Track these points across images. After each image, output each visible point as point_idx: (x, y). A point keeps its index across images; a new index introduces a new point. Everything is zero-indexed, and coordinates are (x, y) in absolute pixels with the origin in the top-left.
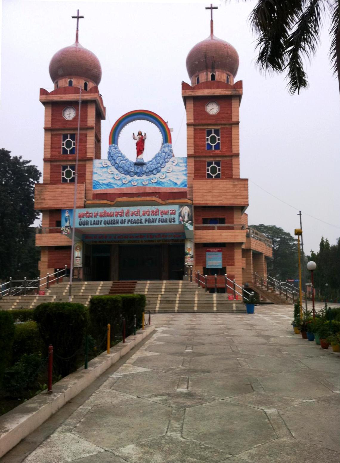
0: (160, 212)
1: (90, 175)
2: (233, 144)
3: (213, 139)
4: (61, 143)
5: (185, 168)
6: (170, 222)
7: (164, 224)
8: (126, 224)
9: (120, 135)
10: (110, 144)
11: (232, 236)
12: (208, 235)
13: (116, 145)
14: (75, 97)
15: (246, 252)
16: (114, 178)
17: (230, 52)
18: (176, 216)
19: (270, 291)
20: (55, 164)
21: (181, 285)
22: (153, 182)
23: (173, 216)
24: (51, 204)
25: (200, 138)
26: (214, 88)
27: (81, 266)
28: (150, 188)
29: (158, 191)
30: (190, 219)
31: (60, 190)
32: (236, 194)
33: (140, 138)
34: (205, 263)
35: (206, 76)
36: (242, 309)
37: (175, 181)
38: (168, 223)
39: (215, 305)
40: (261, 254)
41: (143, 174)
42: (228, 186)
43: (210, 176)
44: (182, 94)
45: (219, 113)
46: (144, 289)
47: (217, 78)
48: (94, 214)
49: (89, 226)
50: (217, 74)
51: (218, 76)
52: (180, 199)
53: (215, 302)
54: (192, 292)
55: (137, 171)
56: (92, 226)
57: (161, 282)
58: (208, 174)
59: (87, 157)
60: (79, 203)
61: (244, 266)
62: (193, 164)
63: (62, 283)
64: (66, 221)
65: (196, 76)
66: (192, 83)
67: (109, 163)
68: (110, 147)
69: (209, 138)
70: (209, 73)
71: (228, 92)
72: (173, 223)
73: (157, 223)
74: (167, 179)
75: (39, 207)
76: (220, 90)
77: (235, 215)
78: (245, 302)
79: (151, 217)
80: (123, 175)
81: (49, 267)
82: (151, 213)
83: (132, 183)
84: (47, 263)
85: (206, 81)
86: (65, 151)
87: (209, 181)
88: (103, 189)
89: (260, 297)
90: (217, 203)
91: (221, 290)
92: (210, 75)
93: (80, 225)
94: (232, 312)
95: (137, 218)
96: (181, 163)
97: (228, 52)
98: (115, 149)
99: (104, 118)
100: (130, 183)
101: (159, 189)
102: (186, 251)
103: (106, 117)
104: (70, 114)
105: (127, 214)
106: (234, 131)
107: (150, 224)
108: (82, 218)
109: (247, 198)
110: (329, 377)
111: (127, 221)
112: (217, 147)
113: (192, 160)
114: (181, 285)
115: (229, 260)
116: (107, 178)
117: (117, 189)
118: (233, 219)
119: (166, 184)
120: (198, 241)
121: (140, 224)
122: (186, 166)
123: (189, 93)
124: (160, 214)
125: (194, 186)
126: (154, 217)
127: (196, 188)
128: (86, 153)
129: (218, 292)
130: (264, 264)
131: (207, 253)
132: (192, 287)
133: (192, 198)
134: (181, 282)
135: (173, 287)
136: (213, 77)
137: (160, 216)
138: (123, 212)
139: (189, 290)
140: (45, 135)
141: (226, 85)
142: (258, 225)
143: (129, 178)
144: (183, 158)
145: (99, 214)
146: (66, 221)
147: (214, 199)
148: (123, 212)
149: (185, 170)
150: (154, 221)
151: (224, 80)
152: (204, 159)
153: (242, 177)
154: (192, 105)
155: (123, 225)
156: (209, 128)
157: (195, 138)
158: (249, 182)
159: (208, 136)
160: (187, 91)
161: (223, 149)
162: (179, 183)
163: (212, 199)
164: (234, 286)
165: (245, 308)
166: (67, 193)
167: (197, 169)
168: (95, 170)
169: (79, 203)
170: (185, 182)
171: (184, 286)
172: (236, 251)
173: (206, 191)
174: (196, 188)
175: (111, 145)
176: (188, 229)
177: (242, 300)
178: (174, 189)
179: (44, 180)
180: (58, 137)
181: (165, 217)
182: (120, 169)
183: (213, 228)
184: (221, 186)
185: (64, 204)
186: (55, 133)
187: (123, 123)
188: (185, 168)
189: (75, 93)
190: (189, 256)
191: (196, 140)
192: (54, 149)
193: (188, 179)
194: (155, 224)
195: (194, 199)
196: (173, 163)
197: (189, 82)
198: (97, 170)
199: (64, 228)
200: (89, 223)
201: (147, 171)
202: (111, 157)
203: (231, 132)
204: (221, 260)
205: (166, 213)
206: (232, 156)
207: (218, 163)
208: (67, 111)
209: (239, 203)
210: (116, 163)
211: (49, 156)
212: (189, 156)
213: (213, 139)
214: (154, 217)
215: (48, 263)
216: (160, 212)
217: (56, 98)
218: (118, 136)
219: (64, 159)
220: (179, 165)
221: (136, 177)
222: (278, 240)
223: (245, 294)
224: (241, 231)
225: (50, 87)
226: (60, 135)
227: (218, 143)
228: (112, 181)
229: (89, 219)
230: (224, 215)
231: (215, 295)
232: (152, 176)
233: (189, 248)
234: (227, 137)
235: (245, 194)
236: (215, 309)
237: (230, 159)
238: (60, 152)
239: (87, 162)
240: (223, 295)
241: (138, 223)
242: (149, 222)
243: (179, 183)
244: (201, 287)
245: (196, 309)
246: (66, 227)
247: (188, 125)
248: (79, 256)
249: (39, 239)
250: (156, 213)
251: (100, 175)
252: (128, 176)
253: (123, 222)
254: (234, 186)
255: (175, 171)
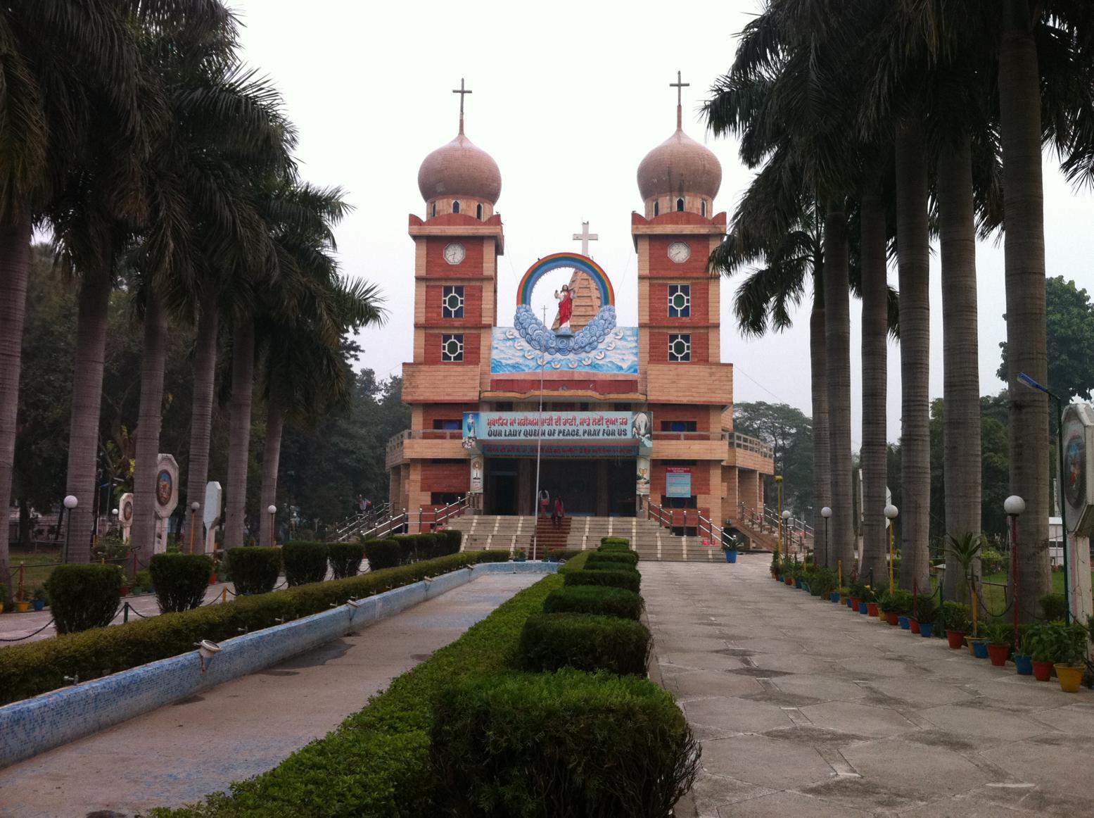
0: (604, 421)
1: (487, 352)
2: (710, 309)
3: (679, 300)
4: (441, 300)
5: (634, 344)
6: (620, 435)
7: (610, 437)
8: (556, 437)
9: (534, 290)
10: (518, 304)
11: (707, 449)
12: (670, 447)
13: (528, 306)
14: (465, 231)
15: (728, 470)
16: (524, 356)
17: (707, 166)
18: (628, 427)
19: (766, 532)
20: (431, 331)
21: (634, 523)
22: (586, 364)
23: (623, 427)
24: (428, 394)
25: (659, 299)
26: (682, 224)
27: (481, 491)
28: (580, 373)
29: (592, 379)
30: (648, 431)
31: (442, 374)
32: (713, 387)
33: (565, 296)
34: (664, 488)
35: (669, 202)
36: (720, 557)
37: (619, 364)
38: (617, 437)
39: (685, 552)
40: (754, 471)
41: (570, 351)
42: (702, 374)
43: (673, 357)
44: (632, 231)
45: (689, 261)
46: (584, 528)
47: (686, 206)
48: (509, 422)
49: (503, 438)
50: (687, 200)
51: (689, 203)
52: (628, 393)
53: (684, 548)
54: (651, 533)
55: (561, 346)
56: (506, 438)
57: (606, 519)
58: (671, 354)
59: (483, 322)
60: (472, 394)
61: (725, 495)
62: (648, 338)
63: (465, 517)
64: (470, 430)
65: (654, 201)
66: (647, 213)
67: (516, 334)
68: (518, 309)
69: (673, 298)
70: (674, 198)
71: (703, 230)
72: (623, 437)
73: (601, 437)
74: (608, 360)
75: (409, 398)
76: (692, 226)
77: (711, 417)
78: (724, 548)
79: (592, 428)
80: (538, 352)
81: (423, 489)
82: (591, 421)
83: (553, 364)
84: (419, 484)
85: (669, 211)
86: (447, 313)
87: (673, 367)
88: (507, 372)
89: (751, 543)
90: (685, 400)
91: (692, 532)
92: (676, 200)
93: (490, 435)
94: (708, 561)
95: (571, 428)
96: (629, 336)
97: (704, 166)
98: (527, 311)
99: (502, 254)
100: (548, 365)
101: (594, 375)
102: (639, 473)
103: (505, 251)
104: (455, 255)
105: (558, 420)
106: (712, 288)
107: (590, 437)
108: (492, 427)
109: (731, 393)
110: (1003, 798)
111: (557, 432)
112: (685, 312)
113: (646, 332)
114: (634, 523)
115: (701, 485)
116: (513, 355)
117: (529, 374)
118: (708, 423)
119: (605, 368)
120: (655, 456)
121: (575, 437)
122: (636, 341)
123: (644, 230)
124: (604, 423)
125: (649, 372)
126: (597, 427)
127: (652, 377)
128: (481, 316)
129: (689, 535)
130: (758, 487)
131: (668, 474)
132: (650, 527)
133: (646, 391)
134: (634, 519)
135: (624, 527)
136: (680, 204)
137: (605, 427)
138: (551, 419)
139: (646, 531)
140: (416, 287)
141: (701, 219)
142: (753, 402)
143: (548, 357)
144: (632, 328)
145: (517, 422)
146: (470, 430)
147: (680, 394)
148: (551, 419)
149: (636, 347)
150: (596, 433)
151: (698, 209)
152: (665, 331)
153: (724, 359)
154: (648, 247)
155: (552, 437)
156: (673, 283)
157: (650, 299)
158: (734, 369)
159: (671, 295)
160: (640, 226)
161: (695, 317)
162: (625, 366)
163: (676, 394)
164: (710, 528)
165: (725, 557)
166: (453, 378)
167: (653, 347)
168: (495, 344)
169: (472, 394)
170: (635, 365)
171: (639, 525)
172: (712, 472)
173: (666, 381)
174: (652, 377)
175: (520, 306)
176: (645, 446)
177: (721, 546)
178: (618, 375)
179: (414, 357)
180: (438, 290)
181: (612, 427)
182: (533, 342)
183: (678, 438)
184: (691, 373)
185: (448, 395)
186: (432, 283)
187: (538, 272)
188: (634, 344)
189: (464, 224)
190: (642, 480)
191: (653, 300)
192: (430, 310)
193: (640, 361)
194: (597, 437)
195: (649, 393)
196: (617, 335)
197: (642, 211)
198: (497, 344)
199: (467, 440)
200: (503, 434)
201: (576, 347)
202: (519, 323)
203: (708, 289)
204: (689, 485)
205: (613, 422)
206: (708, 327)
207: (686, 338)
208: (450, 249)
209: (718, 400)
210: (528, 334)
211: (422, 320)
212: (642, 326)
213: (679, 300)
214: (597, 427)
215: (422, 483)
216: (604, 421)
217: (436, 230)
218: (531, 291)
219: (447, 325)
220: (626, 340)
221: (558, 356)
222: (793, 431)
223: (724, 538)
224: (720, 442)
225: (422, 210)
226: (440, 287)
227: (687, 307)
228: (521, 361)
229: (503, 428)
230: (695, 418)
231: (684, 538)
232: (583, 355)
233: (643, 469)
234: (699, 298)
235: (727, 387)
236: (685, 556)
237: (706, 331)
238: (439, 314)
239: (482, 331)
240: (695, 538)
241: (573, 435)
242: (589, 434)
243: (625, 366)
244: (663, 527)
245: (659, 556)
246: (470, 438)
247: (641, 278)
248: (478, 476)
249: (409, 448)
250: (599, 422)
251: (502, 351)
252: (546, 354)
253: (551, 433)
254: (711, 374)
255: (618, 349)
